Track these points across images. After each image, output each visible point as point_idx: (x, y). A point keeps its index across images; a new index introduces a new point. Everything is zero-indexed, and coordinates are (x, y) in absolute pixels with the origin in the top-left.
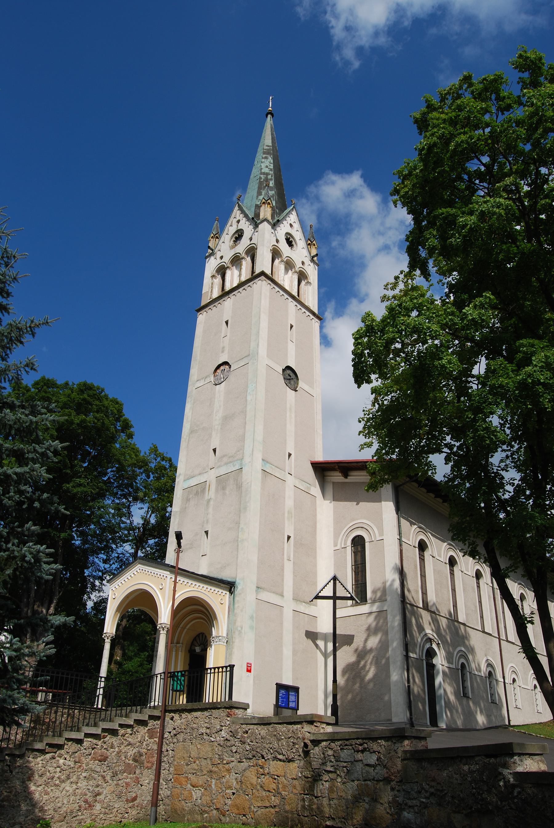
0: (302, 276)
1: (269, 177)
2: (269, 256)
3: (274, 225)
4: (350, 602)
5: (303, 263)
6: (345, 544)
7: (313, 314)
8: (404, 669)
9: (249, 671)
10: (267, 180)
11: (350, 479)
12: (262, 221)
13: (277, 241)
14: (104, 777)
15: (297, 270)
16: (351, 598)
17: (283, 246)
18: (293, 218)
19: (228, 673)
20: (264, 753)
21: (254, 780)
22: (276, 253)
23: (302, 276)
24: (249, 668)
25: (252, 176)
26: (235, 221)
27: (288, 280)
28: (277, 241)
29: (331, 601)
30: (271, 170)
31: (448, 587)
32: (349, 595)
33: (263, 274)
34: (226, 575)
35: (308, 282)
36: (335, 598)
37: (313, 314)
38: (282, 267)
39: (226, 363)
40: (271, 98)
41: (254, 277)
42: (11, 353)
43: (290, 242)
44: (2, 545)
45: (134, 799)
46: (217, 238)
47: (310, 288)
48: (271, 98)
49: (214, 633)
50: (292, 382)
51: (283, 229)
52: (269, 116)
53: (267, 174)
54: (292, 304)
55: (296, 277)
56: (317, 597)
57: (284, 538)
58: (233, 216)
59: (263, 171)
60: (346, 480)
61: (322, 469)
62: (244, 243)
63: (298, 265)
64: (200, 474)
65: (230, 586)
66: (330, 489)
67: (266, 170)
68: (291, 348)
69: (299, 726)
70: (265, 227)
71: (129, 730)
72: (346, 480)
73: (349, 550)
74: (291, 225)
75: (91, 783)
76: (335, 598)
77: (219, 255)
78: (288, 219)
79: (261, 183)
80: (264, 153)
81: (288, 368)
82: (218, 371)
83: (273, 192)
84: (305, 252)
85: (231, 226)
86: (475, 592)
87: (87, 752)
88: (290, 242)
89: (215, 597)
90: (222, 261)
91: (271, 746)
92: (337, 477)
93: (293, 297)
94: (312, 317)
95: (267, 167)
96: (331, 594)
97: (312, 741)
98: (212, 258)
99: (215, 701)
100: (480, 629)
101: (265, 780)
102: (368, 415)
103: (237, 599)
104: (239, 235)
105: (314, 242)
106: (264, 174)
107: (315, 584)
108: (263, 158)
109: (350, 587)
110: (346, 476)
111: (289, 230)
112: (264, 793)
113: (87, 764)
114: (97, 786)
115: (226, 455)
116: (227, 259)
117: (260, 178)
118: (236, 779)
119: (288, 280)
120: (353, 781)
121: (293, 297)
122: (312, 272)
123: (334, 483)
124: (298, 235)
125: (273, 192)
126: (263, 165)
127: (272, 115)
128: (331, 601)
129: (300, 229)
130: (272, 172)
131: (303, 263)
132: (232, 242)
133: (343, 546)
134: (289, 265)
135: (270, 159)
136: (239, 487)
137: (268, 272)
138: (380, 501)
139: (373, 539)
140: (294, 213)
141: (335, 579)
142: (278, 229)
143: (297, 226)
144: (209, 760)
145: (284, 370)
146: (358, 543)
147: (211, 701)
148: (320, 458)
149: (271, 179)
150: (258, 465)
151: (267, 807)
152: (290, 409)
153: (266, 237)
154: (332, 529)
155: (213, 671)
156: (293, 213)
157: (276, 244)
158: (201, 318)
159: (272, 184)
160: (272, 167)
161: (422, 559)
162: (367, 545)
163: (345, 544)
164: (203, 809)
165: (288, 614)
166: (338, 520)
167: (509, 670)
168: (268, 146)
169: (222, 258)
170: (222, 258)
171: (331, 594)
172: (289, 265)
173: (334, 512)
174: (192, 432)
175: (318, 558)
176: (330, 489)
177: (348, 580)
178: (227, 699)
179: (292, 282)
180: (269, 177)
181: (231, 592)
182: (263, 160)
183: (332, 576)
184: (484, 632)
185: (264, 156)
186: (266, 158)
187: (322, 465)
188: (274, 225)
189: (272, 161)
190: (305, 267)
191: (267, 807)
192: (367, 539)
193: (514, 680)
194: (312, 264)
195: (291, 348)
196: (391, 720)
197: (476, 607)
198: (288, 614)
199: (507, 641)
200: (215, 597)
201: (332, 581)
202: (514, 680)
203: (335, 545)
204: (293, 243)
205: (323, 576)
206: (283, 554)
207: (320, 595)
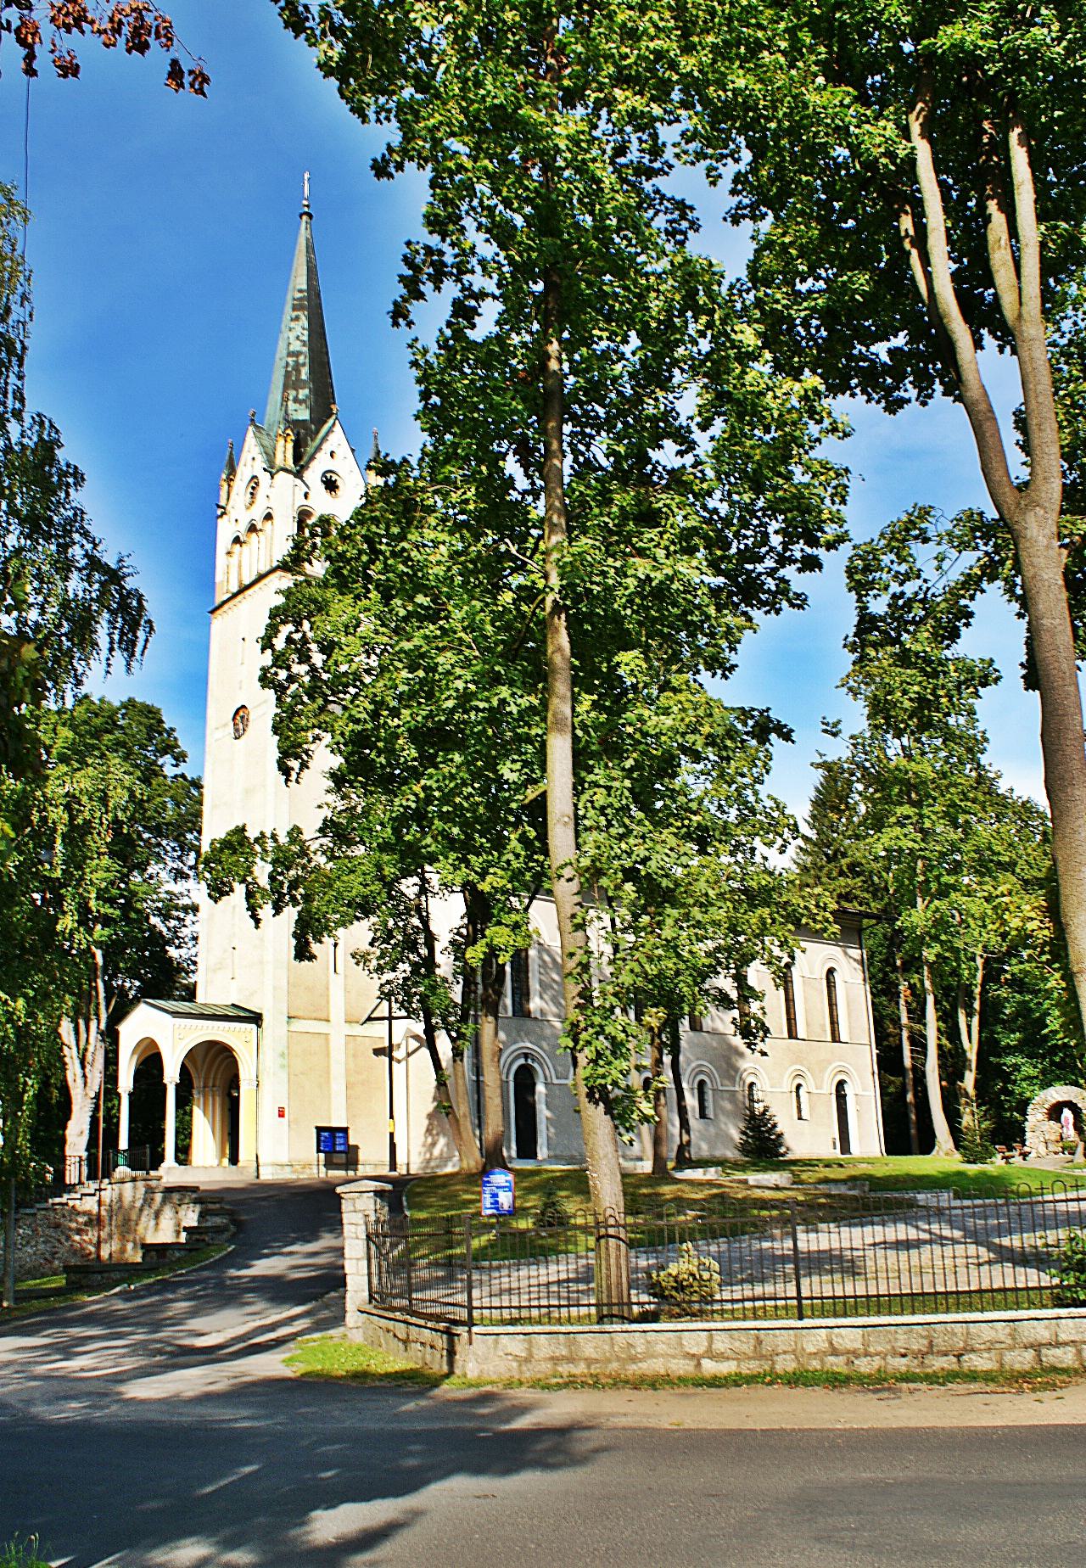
8: (223, 1155)
9: (281, 1115)
18: (336, 440)
40: (307, 176)
42: (441, 330)
48: (307, 176)
51: (313, 474)
53: (297, 354)
56: (369, 1019)
65: (256, 1019)
67: (296, 346)
79: (287, 375)
80: (294, 309)
83: (307, 391)
88: (331, 485)
89: (233, 1035)
125: (307, 391)
127: (310, 216)
130: (305, 349)
135: (304, 322)
140: (338, 428)
143: (343, 450)
152: (1022, 422)
158: (218, 623)
160: (306, 338)
168: (300, 291)
180: (301, 359)
181: (259, 1026)
186: (297, 318)
188: (298, 475)
200: (233, 1035)
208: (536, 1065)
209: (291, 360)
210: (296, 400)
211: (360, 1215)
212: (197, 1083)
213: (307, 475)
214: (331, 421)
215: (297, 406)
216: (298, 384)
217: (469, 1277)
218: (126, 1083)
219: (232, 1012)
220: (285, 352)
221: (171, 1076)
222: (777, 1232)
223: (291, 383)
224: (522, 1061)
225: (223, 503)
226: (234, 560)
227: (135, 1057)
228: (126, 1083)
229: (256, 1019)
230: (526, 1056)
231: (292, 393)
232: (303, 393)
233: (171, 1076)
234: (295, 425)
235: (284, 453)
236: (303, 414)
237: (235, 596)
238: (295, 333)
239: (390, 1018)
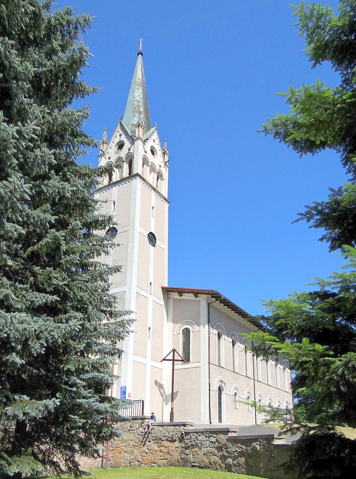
0: (159, 176)
1: (140, 104)
2: (140, 162)
3: (144, 142)
4: (180, 362)
5: (160, 166)
6: (179, 332)
7: (165, 199)
10: (138, 106)
11: (182, 298)
15: (157, 171)
16: (182, 360)
17: (149, 154)
19: (141, 403)
20: (162, 438)
21: (157, 449)
22: (145, 161)
23: (159, 176)
25: (128, 101)
26: (118, 134)
27: (151, 178)
28: (146, 152)
29: (172, 362)
30: (141, 99)
32: (181, 359)
33: (137, 175)
35: (163, 179)
36: (173, 360)
37: (165, 199)
38: (148, 169)
41: (132, 176)
45: (167, 459)
47: (163, 182)
51: (150, 143)
52: (140, 55)
53: (139, 102)
54: (153, 193)
55: (156, 175)
56: (164, 360)
57: (147, 329)
58: (117, 130)
60: (181, 298)
62: (125, 150)
63: (158, 167)
68: (153, 221)
69: (179, 427)
72: (181, 298)
73: (181, 335)
74: (154, 141)
76: (173, 360)
77: (107, 156)
78: (152, 136)
81: (151, 233)
84: (161, 159)
88: (153, 152)
90: (110, 160)
91: (165, 434)
92: (176, 296)
93: (154, 189)
94: (164, 201)
95: (138, 96)
96: (172, 359)
97: (185, 433)
99: (135, 416)
100: (217, 365)
101: (162, 448)
102: (305, 351)
103: (122, 360)
104: (121, 146)
105: (167, 152)
106: (137, 101)
107: (162, 352)
109: (181, 354)
110: (181, 295)
112: (162, 454)
115: (115, 283)
116: (113, 160)
118: (147, 448)
119: (151, 178)
120: (205, 448)
121: (154, 189)
122: (165, 173)
123: (174, 299)
124: (158, 148)
126: (136, 95)
128: (172, 362)
131: (160, 166)
133: (178, 333)
134: (152, 169)
137: (140, 173)
139: (195, 330)
141: (174, 351)
142: (146, 143)
143: (157, 141)
144: (133, 441)
145: (148, 235)
147: (135, 416)
148: (166, 285)
149: (141, 106)
150: (134, 289)
151: (163, 459)
155: (137, 402)
156: (155, 132)
157: (160, 168)
159: (142, 109)
161: (219, 341)
163: (179, 332)
164: (131, 461)
165: (148, 369)
167: (233, 387)
169: (109, 158)
170: (109, 158)
171: (172, 359)
172: (152, 169)
177: (180, 351)
178: (141, 415)
179: (153, 178)
183: (171, 349)
184: (234, 372)
187: (168, 289)
189: (142, 92)
190: (161, 169)
191: (163, 459)
193: (260, 401)
195: (153, 221)
198: (148, 369)
199: (258, 381)
201: (172, 352)
202: (260, 401)
204: (155, 153)
205: (166, 350)
206: (147, 337)
207: (166, 358)
230: (221, 381)
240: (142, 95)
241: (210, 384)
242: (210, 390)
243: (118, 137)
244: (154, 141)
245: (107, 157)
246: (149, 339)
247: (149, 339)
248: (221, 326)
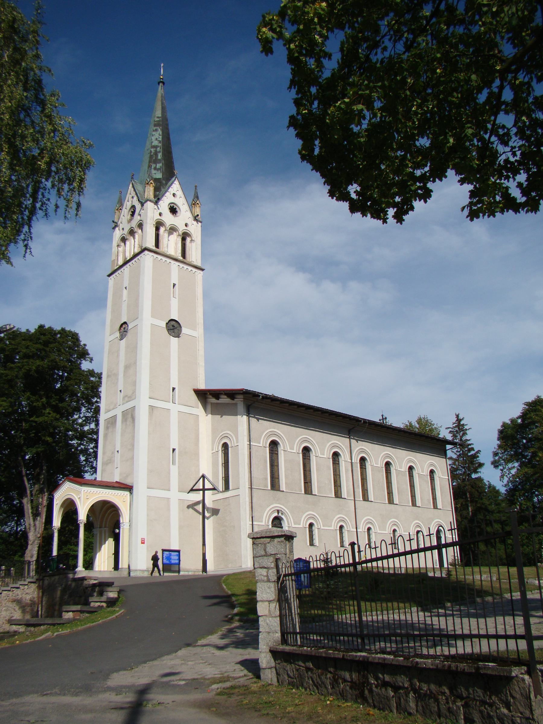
10: (156, 153)
11: (221, 401)
12: (146, 201)
13: (160, 214)
14: (14, 609)
18: (175, 187)
24: (276, 522)
30: (160, 142)
31: (300, 471)
34: (128, 482)
39: (125, 323)
43: (173, 210)
44: (420, 183)
46: (120, 209)
49: (121, 521)
50: (176, 331)
51: (164, 204)
52: (161, 84)
53: (156, 147)
56: (192, 490)
57: (170, 451)
59: (153, 144)
61: (203, 395)
64: (113, 409)
66: (209, 407)
67: (156, 143)
68: (174, 304)
70: (150, 205)
71: (26, 586)
74: (174, 195)
75: (8, 612)
77: (121, 226)
79: (151, 157)
80: (155, 125)
82: (122, 329)
83: (161, 165)
85: (128, 201)
86: (330, 469)
87: (5, 598)
88: (173, 210)
95: (156, 139)
96: (206, 487)
98: (117, 228)
99: (454, 540)
108: (154, 131)
111: (172, 200)
113: (5, 604)
114: (12, 613)
117: (151, 152)
123: (211, 403)
124: (181, 202)
125: (161, 165)
126: (153, 138)
127: (164, 83)
129: (183, 196)
130: (160, 145)
132: (129, 216)
135: (160, 131)
136: (133, 419)
138: (237, 415)
143: (180, 193)
146: (225, 446)
148: (202, 386)
149: (160, 152)
153: (151, 213)
154: (211, 438)
159: (160, 156)
160: (160, 139)
162: (230, 449)
163: (218, 449)
166: (214, 431)
168: (158, 117)
173: (212, 425)
174: (108, 376)
175: (200, 460)
176: (209, 407)
180: (158, 149)
181: (131, 493)
182: (154, 133)
185: (155, 128)
186: (156, 130)
188: (156, 203)
189: (161, 133)
192: (230, 446)
194: (195, 223)
195: (174, 304)
196: (241, 566)
197: (330, 481)
203: (213, 450)
208: (283, 517)
209: (153, 150)
210: (155, 169)
211: (271, 559)
212: (97, 524)
213: (161, 203)
214: (174, 179)
215: (156, 172)
216: (156, 161)
217: (523, 594)
218: (57, 522)
219: (117, 485)
220: (150, 146)
221: (82, 516)
222: (449, 604)
223: (153, 159)
224: (276, 514)
225: (116, 221)
226: (121, 249)
227: (63, 509)
228: (57, 522)
229: (129, 488)
230: (278, 511)
231: (153, 166)
232: (159, 166)
233: (82, 516)
234: (156, 180)
235: (150, 192)
236: (159, 175)
237: (121, 267)
238: (156, 137)
239: (204, 490)
240: (161, 137)
241: (252, 517)
242: (253, 525)
243: (130, 199)
244: (174, 195)
245: (121, 228)
246: (173, 463)
247: (173, 463)
248: (232, 437)
